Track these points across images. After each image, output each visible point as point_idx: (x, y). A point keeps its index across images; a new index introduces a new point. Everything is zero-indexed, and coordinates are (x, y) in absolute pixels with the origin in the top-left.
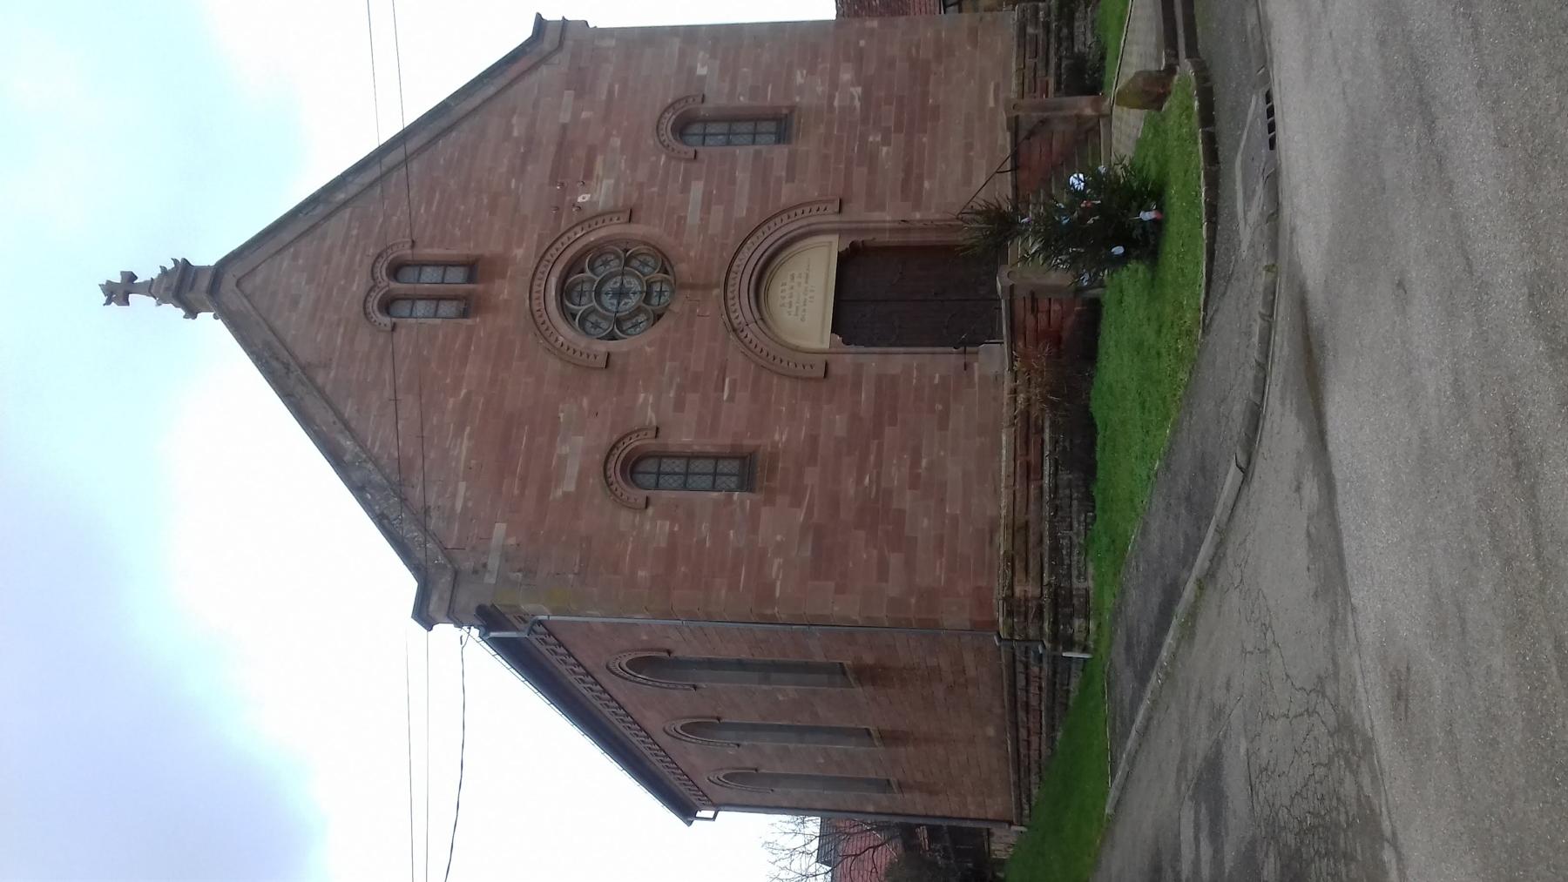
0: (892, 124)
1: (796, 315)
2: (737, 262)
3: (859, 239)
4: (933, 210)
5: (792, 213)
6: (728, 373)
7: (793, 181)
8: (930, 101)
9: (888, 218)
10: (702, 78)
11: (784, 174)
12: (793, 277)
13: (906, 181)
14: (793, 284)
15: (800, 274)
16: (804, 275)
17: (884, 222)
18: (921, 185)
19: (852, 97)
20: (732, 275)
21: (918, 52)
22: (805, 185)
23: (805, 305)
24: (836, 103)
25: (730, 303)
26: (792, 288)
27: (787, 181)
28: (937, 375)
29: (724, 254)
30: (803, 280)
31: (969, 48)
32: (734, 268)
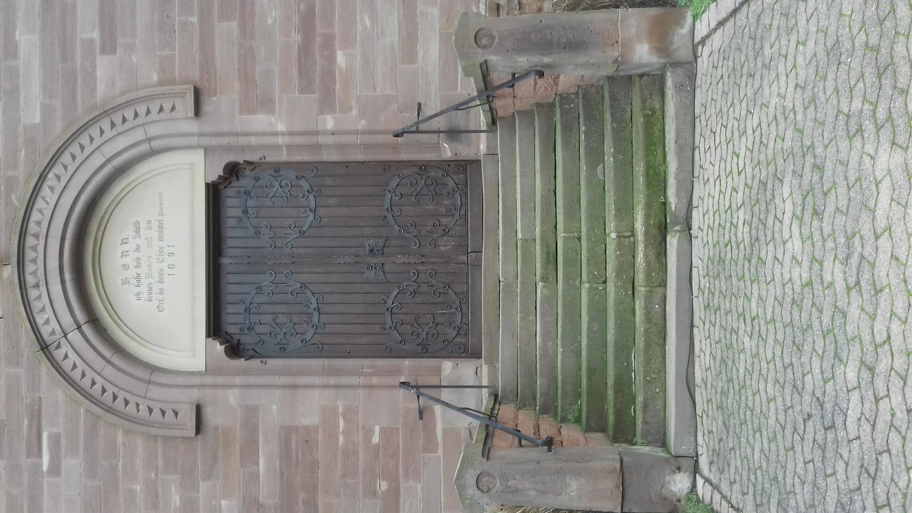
1: (150, 300)
2: (35, 216)
3: (232, 158)
4: (354, 112)
5: (117, 118)
6: (44, 422)
7: (113, 51)
9: (281, 127)
11: (95, 35)
12: (137, 230)
13: (305, 50)
14: (138, 241)
15: (149, 222)
16: (155, 225)
17: (276, 134)
18: (332, 59)
20: (30, 241)
22: (134, 59)
23: (161, 281)
25: (33, 294)
26: (138, 249)
27: (103, 51)
28: (377, 428)
29: (13, 197)
30: (155, 234)
32: (32, 227)
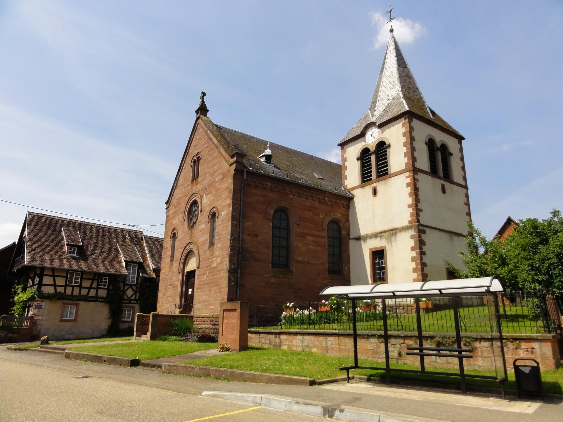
24: (214, 259)
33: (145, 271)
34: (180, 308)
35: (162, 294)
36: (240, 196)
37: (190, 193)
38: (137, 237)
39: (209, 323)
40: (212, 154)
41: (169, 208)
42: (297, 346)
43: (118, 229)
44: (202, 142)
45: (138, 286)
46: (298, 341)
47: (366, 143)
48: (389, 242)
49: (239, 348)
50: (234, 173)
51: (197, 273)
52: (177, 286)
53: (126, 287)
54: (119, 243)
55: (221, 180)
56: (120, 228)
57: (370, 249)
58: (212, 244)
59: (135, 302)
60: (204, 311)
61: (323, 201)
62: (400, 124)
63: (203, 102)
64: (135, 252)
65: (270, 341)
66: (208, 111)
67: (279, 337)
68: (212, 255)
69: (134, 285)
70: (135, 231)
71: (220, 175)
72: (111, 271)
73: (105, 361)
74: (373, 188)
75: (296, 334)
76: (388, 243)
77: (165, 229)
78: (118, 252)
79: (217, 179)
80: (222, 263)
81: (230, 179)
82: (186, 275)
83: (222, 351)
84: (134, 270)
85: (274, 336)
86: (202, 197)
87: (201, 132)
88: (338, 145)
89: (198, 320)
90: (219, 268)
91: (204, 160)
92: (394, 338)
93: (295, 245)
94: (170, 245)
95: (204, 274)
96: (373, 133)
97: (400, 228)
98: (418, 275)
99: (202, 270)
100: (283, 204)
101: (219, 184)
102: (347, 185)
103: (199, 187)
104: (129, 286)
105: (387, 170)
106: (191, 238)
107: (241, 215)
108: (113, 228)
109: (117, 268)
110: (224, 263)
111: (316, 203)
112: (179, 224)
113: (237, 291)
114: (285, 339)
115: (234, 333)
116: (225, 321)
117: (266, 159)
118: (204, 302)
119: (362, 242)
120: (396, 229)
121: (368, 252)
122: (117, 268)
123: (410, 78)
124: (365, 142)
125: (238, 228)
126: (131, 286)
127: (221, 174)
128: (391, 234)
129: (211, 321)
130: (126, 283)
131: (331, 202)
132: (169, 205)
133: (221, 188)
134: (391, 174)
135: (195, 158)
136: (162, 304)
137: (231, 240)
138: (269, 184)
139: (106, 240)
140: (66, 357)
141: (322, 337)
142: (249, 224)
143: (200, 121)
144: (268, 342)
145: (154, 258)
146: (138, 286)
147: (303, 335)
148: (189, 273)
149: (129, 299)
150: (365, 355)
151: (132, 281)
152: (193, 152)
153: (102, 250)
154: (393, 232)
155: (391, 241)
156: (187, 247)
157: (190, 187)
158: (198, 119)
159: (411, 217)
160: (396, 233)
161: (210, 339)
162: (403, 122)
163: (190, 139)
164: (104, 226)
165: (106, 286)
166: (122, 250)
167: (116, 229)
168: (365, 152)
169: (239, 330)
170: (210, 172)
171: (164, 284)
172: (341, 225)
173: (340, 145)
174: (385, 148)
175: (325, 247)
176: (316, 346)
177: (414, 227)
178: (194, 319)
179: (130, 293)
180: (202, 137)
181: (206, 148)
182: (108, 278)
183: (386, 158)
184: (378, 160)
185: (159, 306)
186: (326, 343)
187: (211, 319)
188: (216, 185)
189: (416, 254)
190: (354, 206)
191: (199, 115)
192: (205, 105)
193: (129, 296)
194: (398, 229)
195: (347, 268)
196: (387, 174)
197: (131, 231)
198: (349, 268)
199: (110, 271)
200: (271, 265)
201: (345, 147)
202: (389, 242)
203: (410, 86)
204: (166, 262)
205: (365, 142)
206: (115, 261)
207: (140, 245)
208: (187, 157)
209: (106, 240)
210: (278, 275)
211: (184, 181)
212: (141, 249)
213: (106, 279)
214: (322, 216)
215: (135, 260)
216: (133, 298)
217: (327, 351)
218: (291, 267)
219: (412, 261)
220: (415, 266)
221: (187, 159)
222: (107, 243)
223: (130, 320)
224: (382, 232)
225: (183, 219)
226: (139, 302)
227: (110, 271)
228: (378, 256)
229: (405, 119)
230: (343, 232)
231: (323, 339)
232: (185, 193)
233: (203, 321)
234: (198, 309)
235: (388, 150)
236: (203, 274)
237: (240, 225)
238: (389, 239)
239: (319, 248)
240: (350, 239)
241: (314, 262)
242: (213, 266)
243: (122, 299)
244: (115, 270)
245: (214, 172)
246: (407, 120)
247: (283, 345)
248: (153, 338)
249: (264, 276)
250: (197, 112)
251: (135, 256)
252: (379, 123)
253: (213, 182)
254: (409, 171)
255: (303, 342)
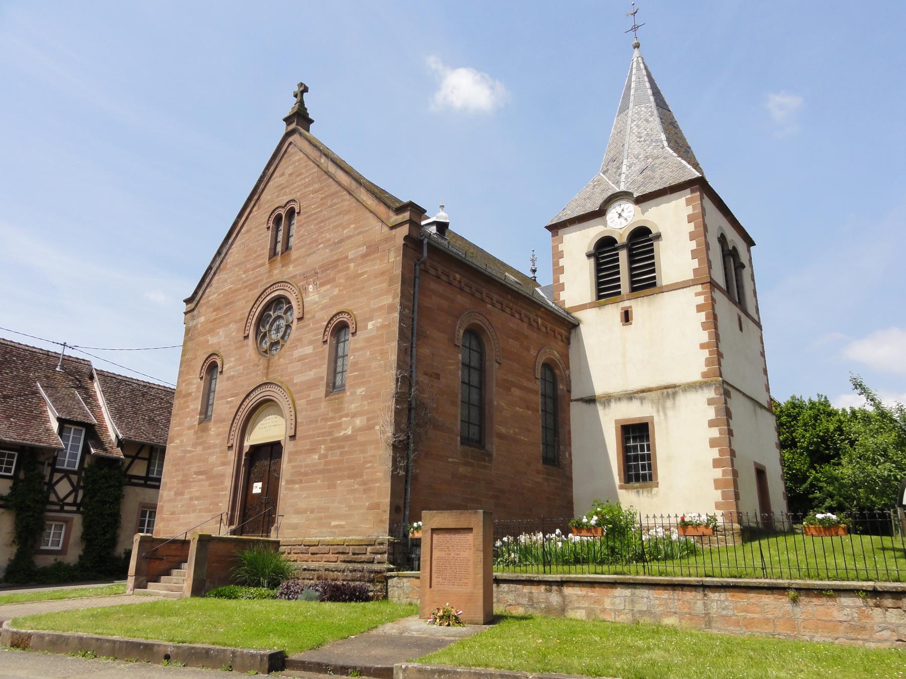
0: (329, 458)
8: (339, 482)
10: (366, 327)
19: (345, 430)
21: (368, 468)
24: (344, 419)
31: (367, 504)
33: (100, 444)
34: (231, 523)
35: (172, 493)
36: (412, 292)
37: (265, 281)
38: (78, 372)
39: (332, 557)
40: (335, 204)
41: (195, 312)
42: (619, 612)
43: (37, 351)
44: (301, 180)
45: (83, 474)
46: (617, 601)
47: (608, 228)
48: (660, 408)
49: (482, 616)
50: (404, 244)
51: (288, 448)
52: (223, 476)
53: (57, 476)
54: (41, 381)
55: (364, 256)
56: (42, 350)
57: (617, 421)
58: (334, 387)
59: (74, 508)
60: (313, 531)
61: (535, 324)
62: (682, 201)
63: (301, 103)
64: (79, 403)
65: (531, 599)
66: (312, 121)
67: (561, 591)
68: (338, 410)
69: (74, 472)
70: (74, 360)
71: (359, 247)
72: (28, 440)
73: (167, 657)
74: (622, 309)
75: (613, 584)
76: (658, 411)
77: (183, 355)
78: (41, 399)
79: (351, 255)
80: (370, 428)
81: (392, 255)
82: (246, 453)
83: (449, 625)
84: (76, 440)
85: (543, 588)
86: (302, 291)
87: (299, 160)
88: (546, 227)
89: (292, 552)
90: (360, 438)
91: (308, 217)
92: (807, 596)
93: (495, 403)
94: (198, 388)
95: (312, 450)
96: (623, 210)
97: (684, 384)
98: (724, 472)
99: (302, 444)
100: (478, 320)
101: (357, 266)
102: (564, 301)
103: (292, 270)
104: (62, 475)
105: (654, 278)
106: (267, 374)
107: (415, 331)
108: (27, 348)
109: (40, 434)
110: (377, 428)
111: (525, 325)
112: (230, 345)
113: (406, 490)
114: (578, 596)
115: (466, 581)
116: (436, 554)
117: (438, 230)
118: (312, 511)
119: (600, 407)
120: (674, 386)
121: (613, 425)
122: (40, 434)
123: (677, 128)
124: (606, 227)
125: (410, 357)
126: (67, 474)
127: (364, 244)
128: (665, 395)
129: (339, 553)
130: (57, 467)
131: (546, 328)
132: (197, 305)
133: (363, 274)
134: (662, 287)
135: (283, 212)
136: (173, 513)
137: (397, 379)
138: (458, 276)
139: (11, 372)
140: (15, 645)
141: (694, 593)
142: (425, 351)
143: (295, 138)
144: (525, 601)
145: (120, 418)
146: (83, 474)
147: (635, 588)
148: (256, 449)
149: (62, 503)
150: (825, 634)
151: (69, 464)
152: (272, 199)
153: (5, 393)
154: (670, 391)
155: (664, 408)
156: (254, 394)
157: (264, 270)
158: (288, 134)
159: (706, 365)
160: (675, 394)
161: (355, 595)
162: (690, 196)
163: (264, 173)
164: (6, 342)
165: (10, 472)
166: (49, 396)
167: (34, 350)
168: (606, 245)
169: (481, 575)
170: (329, 240)
171: (177, 470)
172: (557, 372)
173: (551, 228)
174: (650, 240)
175: (538, 411)
176: (675, 613)
177: (715, 384)
178: (282, 549)
179: (63, 488)
180: (304, 171)
181: (316, 192)
182: (16, 454)
183: (653, 257)
184: (632, 260)
185: (163, 519)
186: (705, 605)
187: (340, 549)
188: (349, 267)
189: (720, 434)
190: (580, 340)
191: (293, 126)
192: (306, 109)
193: (62, 496)
194: (680, 386)
195: (567, 454)
196: (654, 284)
197: (66, 358)
198: (570, 455)
199: (24, 439)
200: (459, 438)
201: (560, 232)
202: (660, 408)
203: (678, 141)
204: (186, 425)
205: (606, 227)
206: (35, 418)
207: (87, 388)
208: (255, 209)
209: (11, 372)
210: (470, 460)
211: (245, 257)
212: (89, 397)
213: (12, 456)
214: (533, 352)
215: (80, 418)
216: (70, 500)
217: (709, 624)
218: (488, 446)
219: (712, 446)
220: (717, 456)
221: (254, 213)
222: (13, 378)
223: (59, 548)
224: (643, 391)
225: (241, 335)
226: (81, 509)
227: (24, 439)
228: (631, 435)
229: (692, 192)
230: (561, 387)
231: (695, 596)
232: (246, 281)
233: (312, 554)
234: (295, 527)
235: (655, 243)
236: (308, 450)
237: (411, 351)
238: (660, 405)
239: (530, 412)
240: (572, 401)
241: (522, 438)
242: (342, 434)
243: (46, 501)
244: (36, 438)
245: (340, 242)
246: (698, 193)
247: (572, 609)
248: (198, 590)
249: (449, 460)
250: (288, 120)
251: (79, 411)
252: (638, 195)
253: (338, 260)
254: (702, 284)
255: (633, 602)
